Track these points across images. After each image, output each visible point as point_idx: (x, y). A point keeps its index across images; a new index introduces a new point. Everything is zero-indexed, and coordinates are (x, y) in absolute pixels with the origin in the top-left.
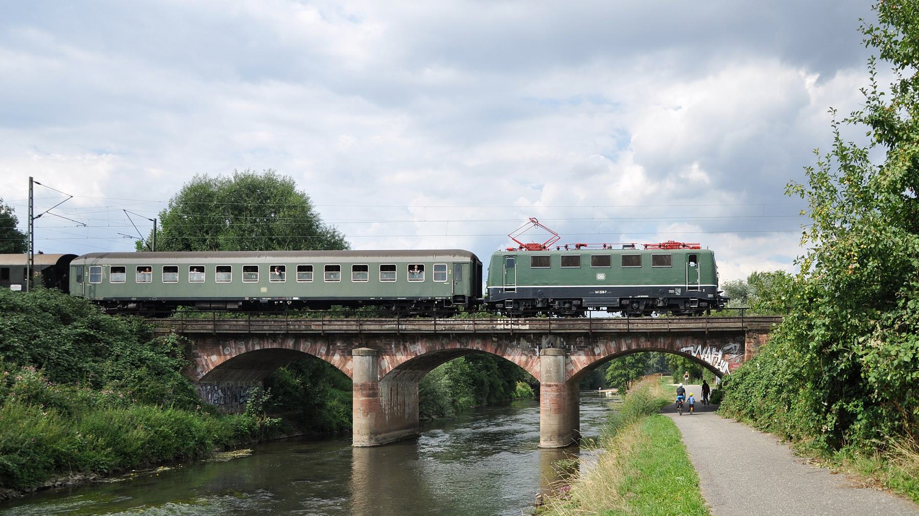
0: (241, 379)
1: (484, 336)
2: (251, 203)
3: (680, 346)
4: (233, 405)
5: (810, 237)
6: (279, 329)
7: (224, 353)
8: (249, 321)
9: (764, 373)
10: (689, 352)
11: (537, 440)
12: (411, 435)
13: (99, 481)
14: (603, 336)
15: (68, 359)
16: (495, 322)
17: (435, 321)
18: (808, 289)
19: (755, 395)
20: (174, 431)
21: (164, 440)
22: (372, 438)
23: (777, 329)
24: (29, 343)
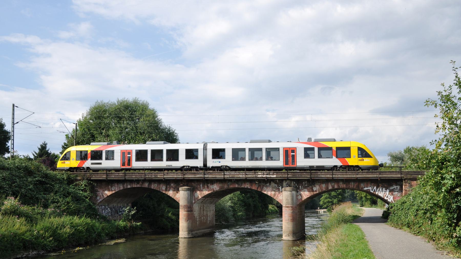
0: (120, 203)
1: (251, 181)
2: (126, 114)
3: (363, 186)
4: (116, 216)
5: (441, 129)
6: (140, 177)
7: (111, 189)
8: (125, 173)
9: (415, 203)
10: (369, 190)
11: (281, 236)
12: (211, 232)
13: (45, 255)
14: (318, 181)
15: (31, 193)
16: (257, 174)
17: (224, 173)
18: (441, 157)
19: (410, 215)
20: (85, 229)
21: (79, 234)
22: (189, 233)
23: (421, 179)
24: (11, 185)
